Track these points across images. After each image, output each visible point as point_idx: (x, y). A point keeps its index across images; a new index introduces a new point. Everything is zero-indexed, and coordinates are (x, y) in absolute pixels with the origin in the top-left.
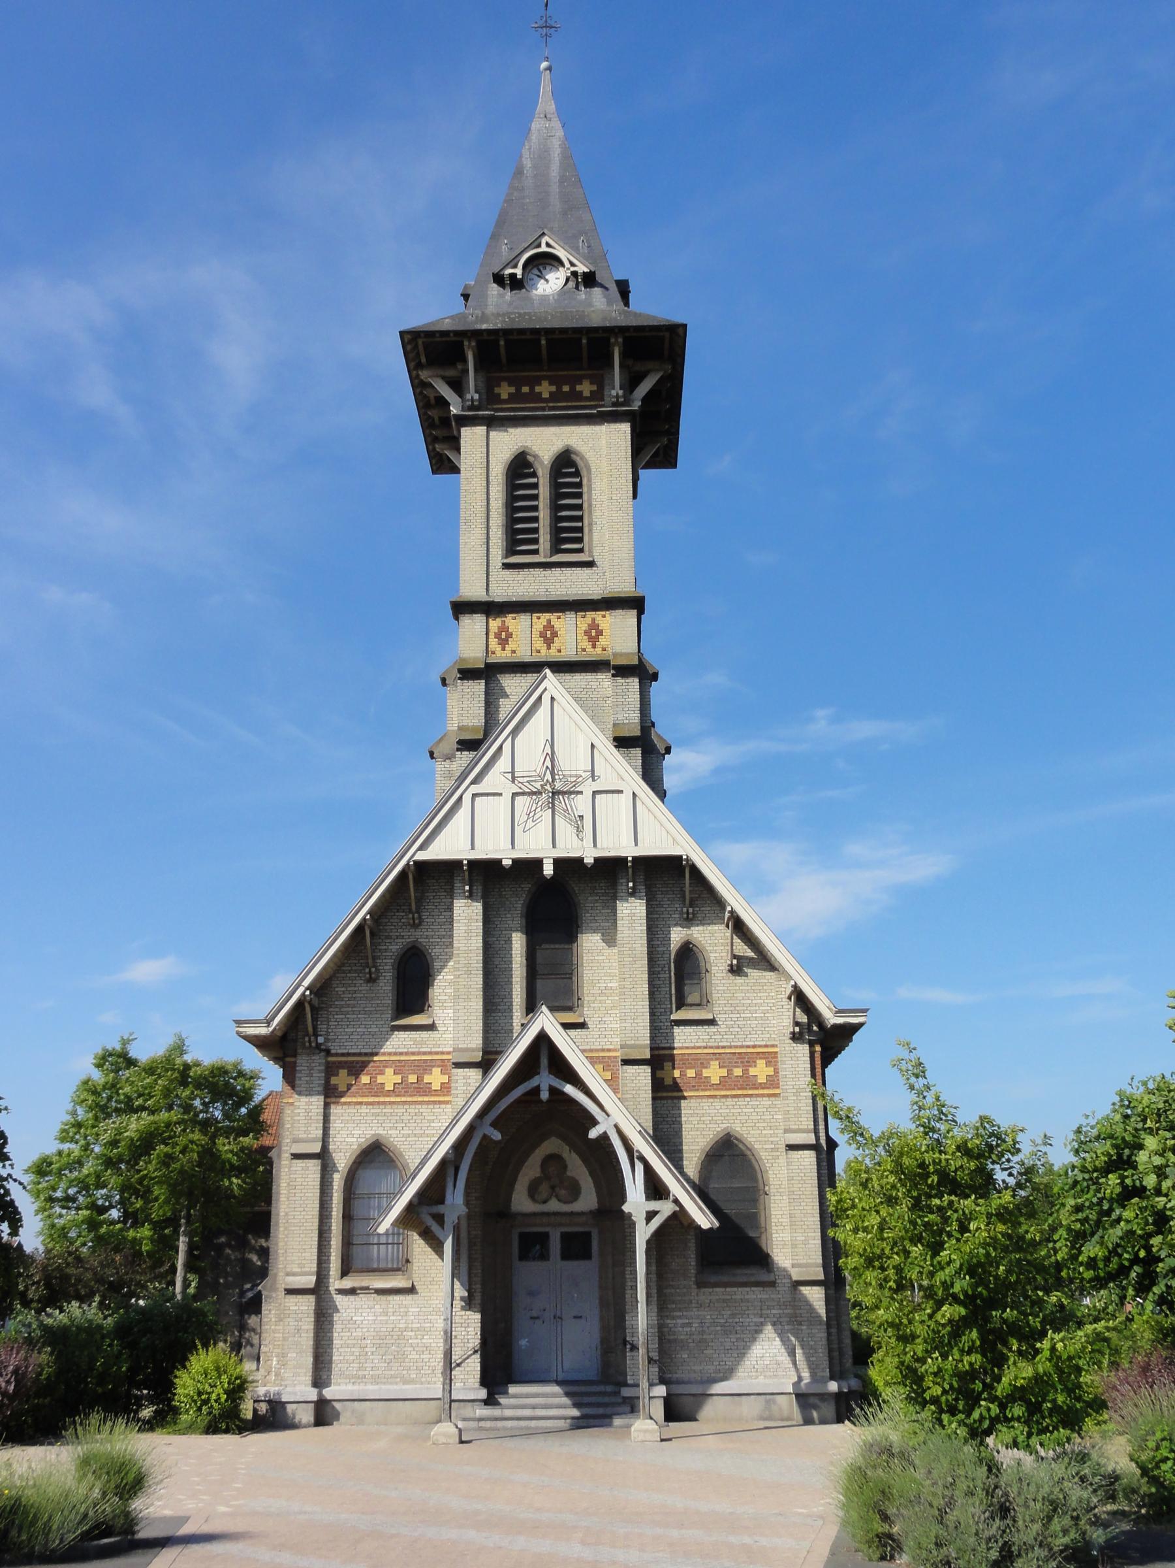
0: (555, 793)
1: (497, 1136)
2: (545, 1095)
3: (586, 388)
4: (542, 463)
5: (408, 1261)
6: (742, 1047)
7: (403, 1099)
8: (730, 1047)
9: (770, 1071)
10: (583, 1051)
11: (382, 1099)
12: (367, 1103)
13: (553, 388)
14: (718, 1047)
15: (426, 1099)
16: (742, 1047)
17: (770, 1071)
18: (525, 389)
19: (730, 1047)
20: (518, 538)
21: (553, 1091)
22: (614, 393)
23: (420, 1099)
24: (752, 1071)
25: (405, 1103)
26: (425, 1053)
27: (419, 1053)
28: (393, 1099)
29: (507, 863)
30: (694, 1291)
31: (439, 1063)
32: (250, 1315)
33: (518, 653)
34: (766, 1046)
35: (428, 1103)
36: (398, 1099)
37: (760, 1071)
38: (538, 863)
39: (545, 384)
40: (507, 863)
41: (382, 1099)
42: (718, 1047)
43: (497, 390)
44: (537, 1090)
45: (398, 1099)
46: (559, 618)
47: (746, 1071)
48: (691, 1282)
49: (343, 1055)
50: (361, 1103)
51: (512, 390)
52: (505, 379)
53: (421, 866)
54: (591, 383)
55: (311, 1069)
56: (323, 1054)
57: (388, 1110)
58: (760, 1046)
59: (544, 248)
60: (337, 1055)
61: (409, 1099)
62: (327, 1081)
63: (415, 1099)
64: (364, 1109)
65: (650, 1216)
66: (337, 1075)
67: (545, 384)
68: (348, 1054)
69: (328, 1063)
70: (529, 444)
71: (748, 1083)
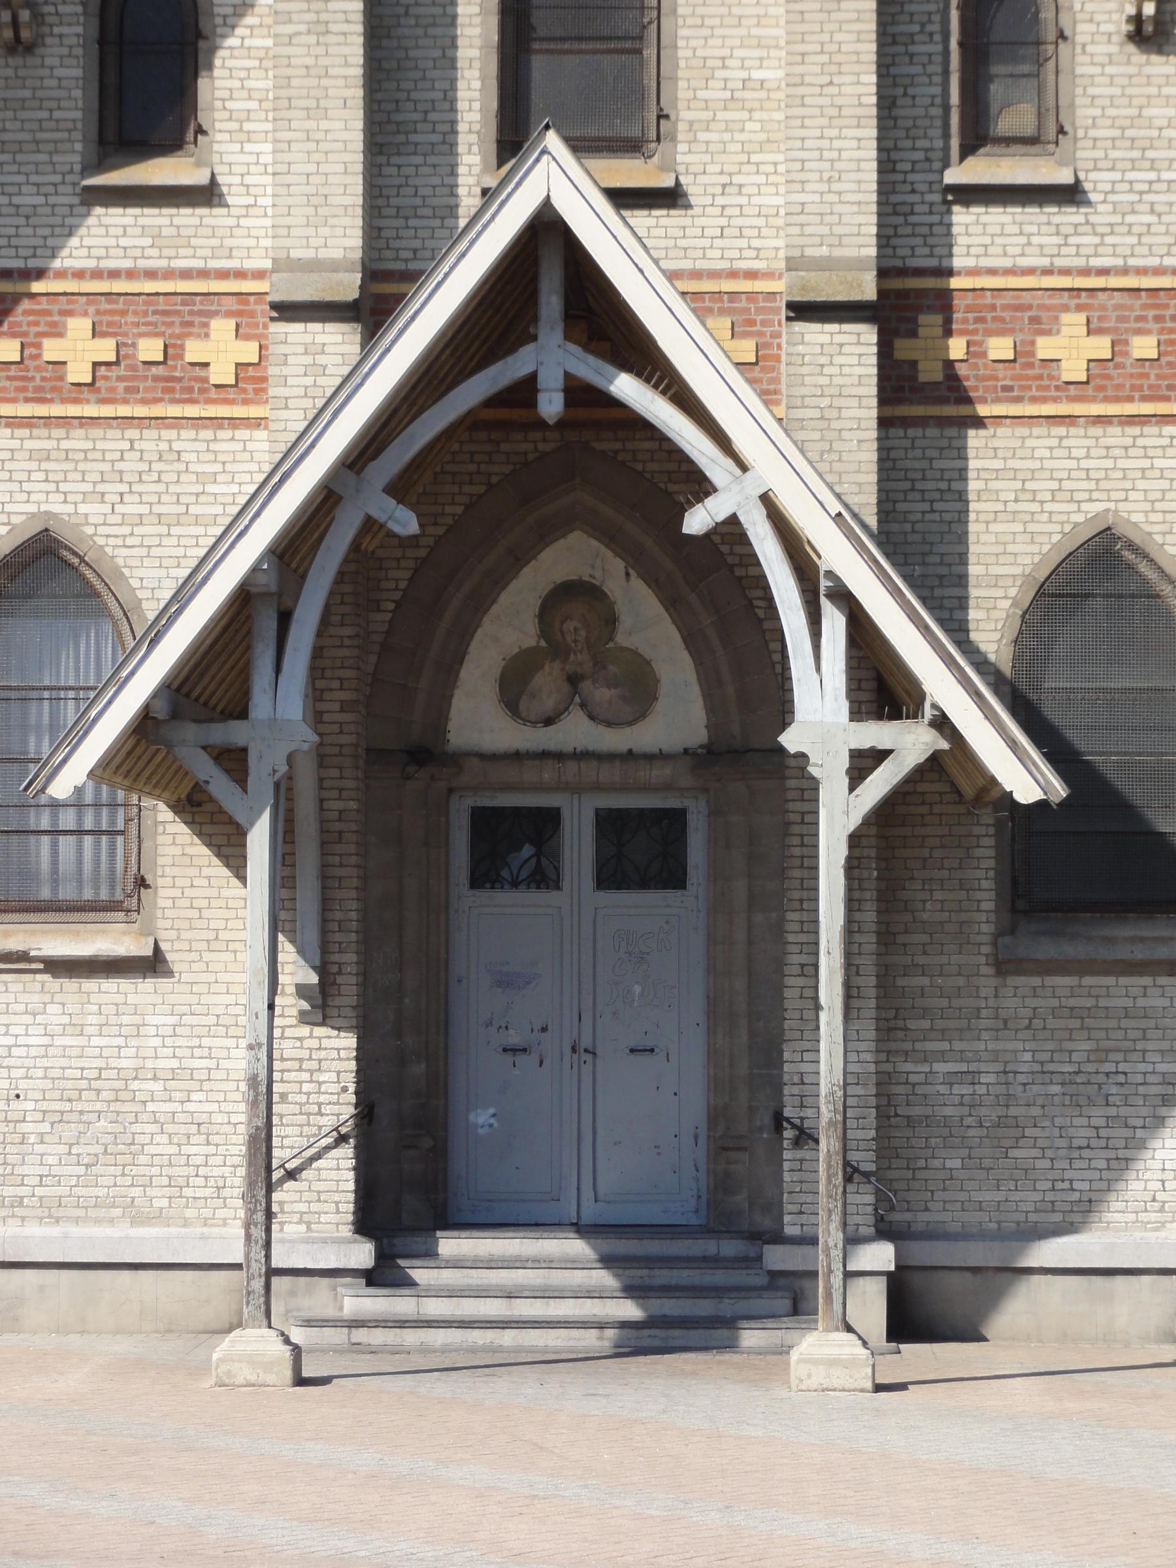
2: (551, 405)
5: (142, 883)
8: (1125, 271)
11: (57, 410)
14: (1085, 272)
15: (192, 411)
19: (1125, 271)
23: (174, 411)
27: (169, 274)
30: (987, 983)
31: (230, 304)
41: (57, 410)
42: (1085, 272)
44: (527, 389)
45: (107, 411)
48: (980, 960)
57: (78, 441)
61: (141, 411)
65: (863, 763)
71: (179, 381)
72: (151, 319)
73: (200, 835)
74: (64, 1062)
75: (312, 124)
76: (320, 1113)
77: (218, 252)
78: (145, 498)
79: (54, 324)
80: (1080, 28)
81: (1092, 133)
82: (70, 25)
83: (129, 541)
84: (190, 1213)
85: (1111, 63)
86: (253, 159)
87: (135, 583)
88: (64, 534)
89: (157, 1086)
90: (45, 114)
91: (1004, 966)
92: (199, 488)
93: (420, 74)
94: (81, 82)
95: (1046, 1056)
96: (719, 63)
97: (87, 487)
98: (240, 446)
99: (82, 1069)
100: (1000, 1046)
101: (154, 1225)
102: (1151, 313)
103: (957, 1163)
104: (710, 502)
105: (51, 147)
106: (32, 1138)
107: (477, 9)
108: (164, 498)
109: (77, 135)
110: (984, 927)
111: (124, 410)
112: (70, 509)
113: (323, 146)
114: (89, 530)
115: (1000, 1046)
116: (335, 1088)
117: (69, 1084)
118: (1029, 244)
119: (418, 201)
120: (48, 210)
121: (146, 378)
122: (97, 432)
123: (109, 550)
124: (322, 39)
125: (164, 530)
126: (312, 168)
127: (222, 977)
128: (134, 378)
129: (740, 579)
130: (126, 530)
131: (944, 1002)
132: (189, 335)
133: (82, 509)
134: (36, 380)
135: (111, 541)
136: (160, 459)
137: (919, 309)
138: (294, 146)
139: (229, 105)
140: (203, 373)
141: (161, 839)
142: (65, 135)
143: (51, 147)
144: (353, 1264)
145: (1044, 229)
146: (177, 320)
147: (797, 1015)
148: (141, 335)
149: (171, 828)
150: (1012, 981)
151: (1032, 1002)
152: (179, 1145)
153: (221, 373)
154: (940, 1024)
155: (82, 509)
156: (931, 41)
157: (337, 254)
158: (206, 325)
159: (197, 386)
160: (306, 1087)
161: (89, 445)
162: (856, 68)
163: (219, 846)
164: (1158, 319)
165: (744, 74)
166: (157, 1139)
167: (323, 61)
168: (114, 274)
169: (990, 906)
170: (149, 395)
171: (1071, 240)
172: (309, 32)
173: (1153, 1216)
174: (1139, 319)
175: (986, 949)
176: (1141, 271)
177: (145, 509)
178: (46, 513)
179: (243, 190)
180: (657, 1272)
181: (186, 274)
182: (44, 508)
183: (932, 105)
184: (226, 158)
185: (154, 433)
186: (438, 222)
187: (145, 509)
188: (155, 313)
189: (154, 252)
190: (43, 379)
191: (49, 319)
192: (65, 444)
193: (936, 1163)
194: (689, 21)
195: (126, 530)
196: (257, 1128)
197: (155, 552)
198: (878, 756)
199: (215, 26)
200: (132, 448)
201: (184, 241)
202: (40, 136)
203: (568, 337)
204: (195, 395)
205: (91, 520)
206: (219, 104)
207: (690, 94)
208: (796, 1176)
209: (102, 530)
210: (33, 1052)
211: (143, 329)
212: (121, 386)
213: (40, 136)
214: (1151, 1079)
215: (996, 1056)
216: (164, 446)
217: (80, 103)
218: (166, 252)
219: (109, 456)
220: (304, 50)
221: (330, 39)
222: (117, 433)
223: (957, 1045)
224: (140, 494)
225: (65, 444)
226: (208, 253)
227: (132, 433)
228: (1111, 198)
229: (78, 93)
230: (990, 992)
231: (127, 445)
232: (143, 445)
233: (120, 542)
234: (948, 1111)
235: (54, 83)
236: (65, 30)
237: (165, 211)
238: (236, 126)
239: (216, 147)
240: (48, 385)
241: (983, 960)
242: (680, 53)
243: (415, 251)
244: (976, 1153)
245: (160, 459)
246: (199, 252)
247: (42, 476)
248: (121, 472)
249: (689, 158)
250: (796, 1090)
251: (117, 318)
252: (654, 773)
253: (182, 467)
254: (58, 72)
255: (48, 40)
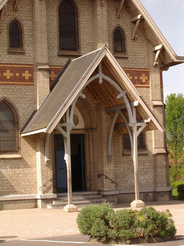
2: (101, 82)
6: (137, 68)
7: (14, 83)
8: (133, 68)
9: (30, 75)
10: (123, 68)
14: (129, 68)
15: (23, 83)
16: (137, 68)
17: (30, 75)
19: (133, 68)
21: (104, 80)
24: (23, 75)
25: (14, 84)
26: (22, 64)
27: (19, 64)
28: (10, 83)
30: (122, 157)
31: (28, 69)
34: (145, 69)
37: (27, 75)
42: (129, 68)
44: (98, 79)
45: (12, 83)
47: (21, 75)
48: (121, 155)
58: (143, 69)
61: (16, 83)
63: (19, 83)
65: (138, 127)
66: (29, 73)
71: (22, 79)
72: (17, 70)
73: (26, 141)
74: (10, 172)
75: (41, 45)
76: (48, 178)
77: (26, 62)
78: (17, 95)
79: (5, 71)
80: (127, 38)
81: (129, 51)
82: (5, 30)
83: (15, 101)
84: (27, 192)
85: (131, 43)
86: (30, 49)
87: (16, 106)
88: (7, 100)
89: (22, 175)
90: (2, 42)
91: (123, 155)
92: (24, 93)
93: (50, 39)
94: (7, 38)
95: (129, 166)
96: (86, 40)
97: (10, 93)
98: (29, 88)
99: (12, 173)
100: (123, 165)
101: (22, 194)
102: (136, 74)
103: (119, 180)
104: (120, 94)
105: (3, 46)
106: (6, 183)
107: (56, 31)
108: (20, 95)
109: (7, 45)
110: (121, 150)
111: (14, 83)
112: (7, 96)
113: (43, 48)
114: (10, 99)
115: (123, 165)
116: (50, 174)
117: (11, 175)
118: (123, 64)
119: (50, 56)
120: (3, 55)
121: (17, 78)
122: (11, 86)
123: (13, 102)
124: (42, 34)
125: (20, 99)
126: (41, 51)
127: (30, 160)
128: (15, 78)
129: (91, 106)
130: (15, 99)
131: (117, 160)
132: (22, 73)
133: (9, 96)
134: (4, 79)
135: (13, 101)
136: (19, 90)
138: (39, 48)
139: (26, 42)
140: (24, 78)
141: (21, 141)
142: (5, 45)
143: (3, 46)
144: (106, 192)
145: (124, 63)
146: (21, 71)
147: (105, 162)
148: (16, 72)
149: (22, 140)
150: (124, 157)
151: (127, 160)
152: (25, 183)
153: (27, 78)
154: (117, 163)
155: (9, 96)
156: (111, 39)
157: (45, 62)
158: (25, 71)
159: (23, 80)
160: (46, 174)
161: (10, 87)
162: (106, 41)
163: (29, 142)
164: (137, 74)
165: (88, 41)
166: (22, 182)
167: (42, 37)
169: (121, 148)
170: (17, 81)
171: (127, 64)
172: (40, 33)
173: (141, 186)
174: (135, 74)
175: (121, 153)
176: (135, 68)
177: (17, 96)
178: (5, 97)
179: (28, 53)
180: (89, 196)
181: (22, 64)
182: (4, 96)
183: (6, 50)
184: (26, 49)
185: (18, 86)
186: (52, 59)
187: (17, 96)
188: (18, 69)
189: (17, 61)
190: (3, 78)
191: (4, 70)
192: (6, 87)
193: (117, 181)
194: (82, 34)
195: (15, 99)
196: (70, 178)
197: (19, 102)
199: (24, 31)
200: (15, 88)
201: (21, 60)
202: (2, 45)
203: (102, 73)
204: (23, 81)
205: (10, 98)
206: (25, 42)
207: (82, 44)
208: (106, 183)
209: (12, 99)
210: (5, 171)
211: (16, 72)
212: (14, 79)
213: (2, 45)
214: (140, 169)
215: (123, 167)
216: (19, 88)
217: (7, 41)
218: (19, 61)
219: (12, 89)
220: (40, 35)
221: (43, 34)
222: (13, 86)
223: (119, 166)
224: (17, 94)
225: (6, 87)
226: (24, 62)
227: (15, 86)
228: (131, 59)
229: (6, 39)
230: (122, 159)
231: (15, 88)
232: (17, 88)
233: (14, 101)
234: (118, 174)
235: (3, 38)
236: (4, 30)
237: (19, 56)
238: (27, 45)
239: (25, 47)
240: (4, 79)
241: (121, 155)
242: (81, 38)
243: (50, 62)
244: (121, 179)
245: (19, 90)
246: (23, 62)
247: (3, 91)
248: (14, 91)
249: (83, 52)
250: (105, 172)
251: (13, 70)
252: (79, 132)
253: (22, 91)
254: (4, 36)
255: (2, 32)
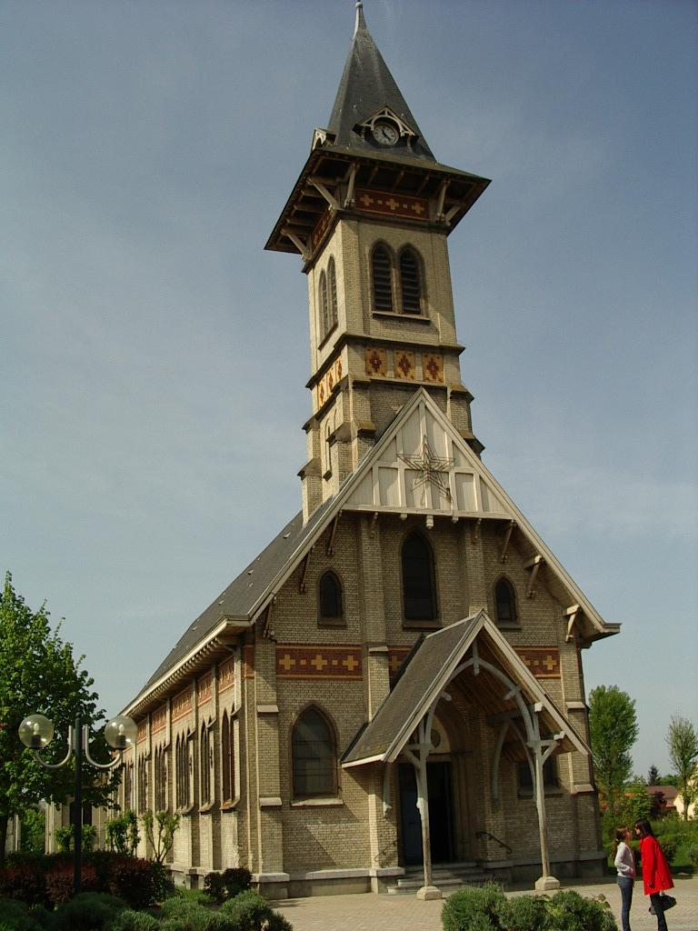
0: (432, 473)
1: (508, 697)
2: (477, 671)
3: (418, 208)
4: (392, 252)
5: (339, 787)
11: (314, 676)
12: (304, 679)
13: (372, 201)
18: (380, 202)
19: (531, 647)
20: (381, 298)
22: (439, 214)
27: (338, 645)
29: (404, 516)
32: (62, 852)
33: (416, 378)
34: (551, 647)
35: (346, 680)
36: (326, 677)
37: (350, 663)
38: (424, 517)
39: (392, 201)
40: (404, 516)
41: (314, 676)
43: (362, 199)
46: (410, 355)
48: (515, 796)
49: (286, 644)
50: (300, 679)
51: (372, 201)
52: (367, 193)
53: (345, 513)
54: (421, 206)
55: (266, 653)
56: (274, 643)
57: (319, 684)
59: (386, 115)
60: (281, 644)
62: (277, 664)
64: (303, 683)
65: (544, 749)
67: (392, 201)
68: (290, 644)
69: (276, 650)
70: (384, 238)
91: (520, 797)
110: (515, 789)
137: (316, 654)
168: (325, 645)
198: (547, 747)
